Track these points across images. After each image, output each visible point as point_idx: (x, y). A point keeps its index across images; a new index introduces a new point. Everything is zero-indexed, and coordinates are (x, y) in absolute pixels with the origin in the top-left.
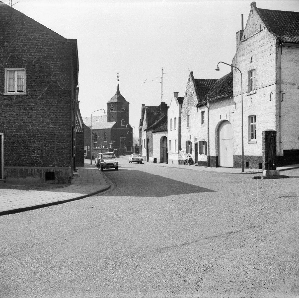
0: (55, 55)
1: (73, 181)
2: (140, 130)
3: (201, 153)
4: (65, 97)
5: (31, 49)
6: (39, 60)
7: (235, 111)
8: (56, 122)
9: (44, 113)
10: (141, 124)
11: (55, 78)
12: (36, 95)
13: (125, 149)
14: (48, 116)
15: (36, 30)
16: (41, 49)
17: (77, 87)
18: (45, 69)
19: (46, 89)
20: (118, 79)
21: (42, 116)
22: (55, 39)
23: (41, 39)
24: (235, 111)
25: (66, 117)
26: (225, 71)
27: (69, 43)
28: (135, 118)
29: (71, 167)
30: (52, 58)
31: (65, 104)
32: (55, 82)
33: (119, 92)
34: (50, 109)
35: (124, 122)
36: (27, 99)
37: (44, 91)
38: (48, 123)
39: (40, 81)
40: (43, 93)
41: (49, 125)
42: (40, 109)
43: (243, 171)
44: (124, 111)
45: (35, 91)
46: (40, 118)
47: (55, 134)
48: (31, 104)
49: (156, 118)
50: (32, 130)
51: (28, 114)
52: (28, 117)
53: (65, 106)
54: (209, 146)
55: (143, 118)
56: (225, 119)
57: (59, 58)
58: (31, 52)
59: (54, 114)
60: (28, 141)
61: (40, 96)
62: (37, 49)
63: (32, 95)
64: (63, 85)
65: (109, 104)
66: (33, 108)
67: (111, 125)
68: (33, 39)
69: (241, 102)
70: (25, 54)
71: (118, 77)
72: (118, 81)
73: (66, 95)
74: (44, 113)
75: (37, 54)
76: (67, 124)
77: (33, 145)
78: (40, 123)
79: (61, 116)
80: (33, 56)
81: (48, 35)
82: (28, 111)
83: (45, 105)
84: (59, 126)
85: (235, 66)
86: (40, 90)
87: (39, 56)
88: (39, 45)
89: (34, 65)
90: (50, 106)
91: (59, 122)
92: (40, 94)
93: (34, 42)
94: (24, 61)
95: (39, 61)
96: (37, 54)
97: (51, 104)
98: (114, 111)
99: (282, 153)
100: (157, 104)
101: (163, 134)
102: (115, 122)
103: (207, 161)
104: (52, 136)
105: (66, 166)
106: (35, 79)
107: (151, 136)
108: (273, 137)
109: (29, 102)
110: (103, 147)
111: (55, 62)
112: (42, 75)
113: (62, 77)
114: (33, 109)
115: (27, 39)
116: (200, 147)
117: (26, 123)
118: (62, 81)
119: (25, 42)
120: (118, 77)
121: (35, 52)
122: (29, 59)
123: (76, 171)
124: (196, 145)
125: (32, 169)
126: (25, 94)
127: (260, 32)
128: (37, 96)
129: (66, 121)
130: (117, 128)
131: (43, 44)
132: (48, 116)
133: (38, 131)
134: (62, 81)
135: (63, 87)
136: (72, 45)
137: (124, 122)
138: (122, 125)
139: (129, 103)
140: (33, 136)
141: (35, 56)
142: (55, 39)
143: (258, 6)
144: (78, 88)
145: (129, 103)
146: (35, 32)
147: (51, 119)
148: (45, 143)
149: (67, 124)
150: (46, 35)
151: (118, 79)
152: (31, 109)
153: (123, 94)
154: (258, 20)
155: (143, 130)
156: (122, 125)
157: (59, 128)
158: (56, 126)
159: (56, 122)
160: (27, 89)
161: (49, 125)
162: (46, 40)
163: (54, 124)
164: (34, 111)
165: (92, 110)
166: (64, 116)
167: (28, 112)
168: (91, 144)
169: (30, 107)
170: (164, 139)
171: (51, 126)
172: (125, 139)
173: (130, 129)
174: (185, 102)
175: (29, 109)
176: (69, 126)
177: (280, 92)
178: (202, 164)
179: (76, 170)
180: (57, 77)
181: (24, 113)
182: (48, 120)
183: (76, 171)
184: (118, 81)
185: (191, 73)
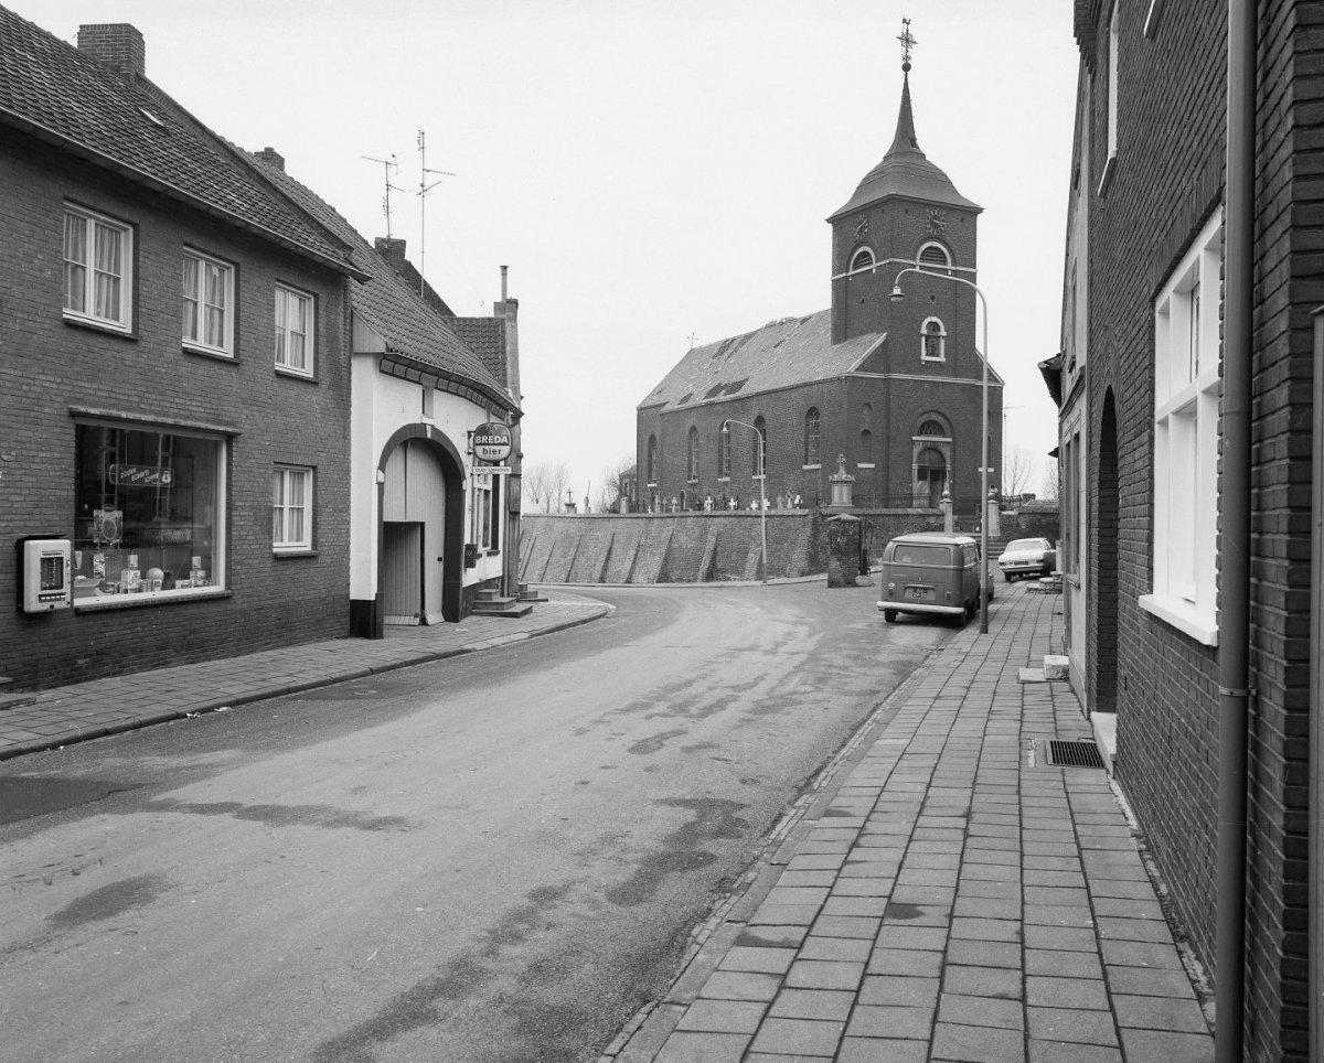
20: (907, 58)
33: (913, 141)
35: (943, 333)
44: (945, 262)
65: (837, 221)
67: (847, 360)
71: (907, 40)
72: (907, 68)
98: (875, 264)
99: (393, 617)
102: (880, 331)
103: (1051, 497)
116: (1154, 28)
120: (907, 40)
130: (888, 370)
137: (943, 333)
138: (924, 357)
139: (980, 210)
145: (980, 210)
151: (907, 58)
153: (928, 142)
156: (924, 357)
168: (277, 344)
172: (947, 453)
184: (907, 68)
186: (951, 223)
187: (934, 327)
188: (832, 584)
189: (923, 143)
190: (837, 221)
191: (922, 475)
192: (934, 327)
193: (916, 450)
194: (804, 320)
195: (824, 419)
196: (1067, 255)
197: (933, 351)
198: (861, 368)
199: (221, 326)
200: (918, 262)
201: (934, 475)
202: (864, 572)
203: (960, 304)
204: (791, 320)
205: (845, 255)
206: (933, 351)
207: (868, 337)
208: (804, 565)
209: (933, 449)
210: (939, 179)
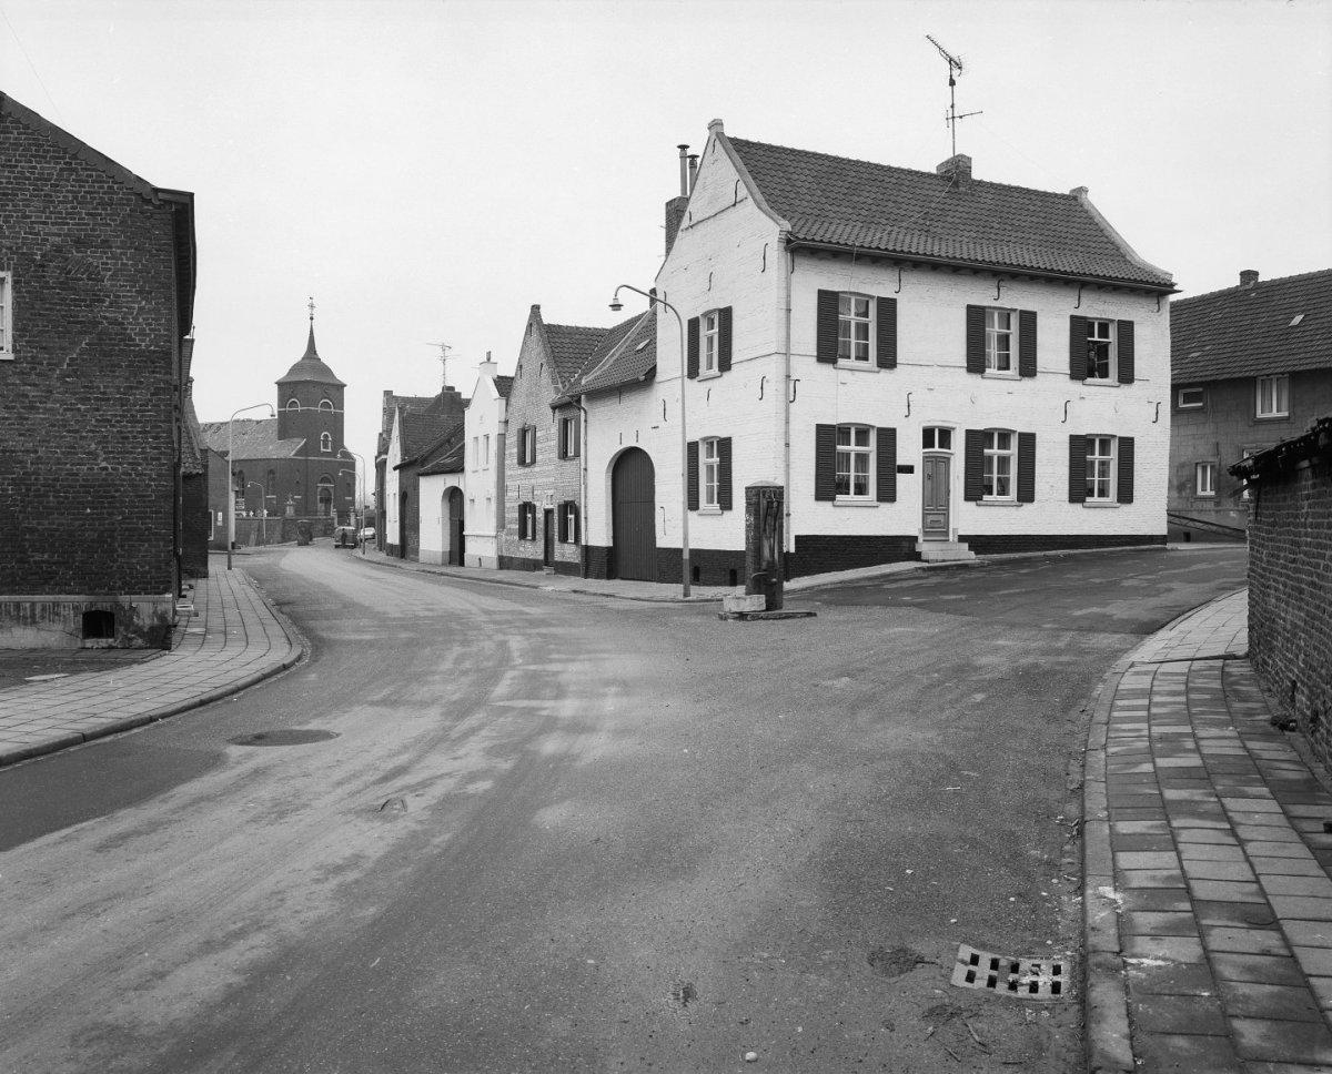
0: (118, 236)
1: (175, 638)
2: (381, 467)
3: (564, 539)
4: (154, 372)
5: (30, 211)
6: (59, 249)
7: (662, 424)
8: (119, 453)
9: (77, 422)
10: (383, 449)
11: (115, 312)
12: (49, 364)
13: (333, 519)
14: (92, 431)
15: (48, 151)
16: (67, 213)
17: (187, 337)
18: (82, 279)
19: (83, 345)
21: (69, 431)
22: (116, 186)
23: (68, 181)
24: (662, 424)
25: (155, 438)
26: (636, 306)
27: (164, 201)
28: (362, 431)
29: (171, 595)
30: (106, 244)
31: (152, 395)
32: (114, 322)
34: (98, 410)
36: (14, 373)
37: (78, 351)
38: (93, 455)
39: (63, 316)
40: (75, 356)
41: (95, 459)
42: (65, 410)
43: (686, 595)
45: (45, 348)
46: (65, 436)
47: (116, 491)
48: (32, 392)
49: (431, 433)
50: (33, 478)
51: (22, 424)
52: (20, 435)
53: (150, 400)
54: (586, 518)
55: (388, 431)
56: (634, 444)
57: (129, 248)
58: (32, 223)
59: (113, 426)
60: (20, 512)
61: (65, 367)
62: (51, 212)
63: (34, 361)
64: (145, 335)
65: (280, 384)
66: (38, 404)
67: (289, 450)
68: (38, 179)
69: (680, 401)
70: (8, 227)
71: (312, 306)
73: (156, 367)
74: (77, 422)
75: (54, 229)
76: (159, 459)
77: (39, 524)
78: (63, 453)
79: (140, 433)
80: (38, 234)
81: (93, 170)
82: (19, 413)
83: (83, 395)
84: (129, 464)
85: (663, 299)
86: (62, 349)
87: (59, 235)
88: (59, 202)
89: (42, 266)
90: (97, 399)
91: (132, 453)
92: (64, 360)
93: (42, 190)
94: (4, 250)
95: (61, 251)
96: (54, 229)
97: (104, 393)
98: (299, 409)
100: (432, 391)
101: (451, 481)
104: (106, 497)
105: (156, 594)
106: (47, 309)
107: (416, 488)
108: (775, 504)
109: (26, 384)
110: (266, 512)
111: (115, 250)
112: (72, 300)
113: (141, 309)
114: (38, 408)
115: (15, 178)
117: (13, 452)
118: (141, 320)
119: (8, 189)
120: (312, 306)
121: (45, 223)
122: (24, 244)
123: (185, 597)
124: (548, 512)
125: (33, 604)
126: (11, 357)
127: (734, 205)
128: (53, 366)
129: (155, 448)
131: (76, 198)
132: (92, 431)
133: (57, 480)
134: (141, 320)
135: (144, 341)
136: (177, 211)
140: (40, 496)
141: (46, 234)
142: (116, 186)
143: (729, 132)
144: (193, 341)
146: (45, 157)
147: (103, 441)
148: (81, 519)
149: (159, 459)
150: (86, 169)
152: (32, 408)
153: (323, 354)
154: (724, 175)
155: (389, 467)
156: (322, 449)
157: (133, 469)
158: (120, 464)
159: (119, 453)
160: (15, 340)
161: (95, 459)
162: (84, 187)
163: (114, 458)
164: (42, 416)
165: (230, 386)
166: (149, 432)
167: (21, 418)
169: (27, 401)
170: (454, 497)
171: (104, 464)
172: (332, 491)
173: (349, 463)
174: (520, 389)
175: (24, 408)
176: (164, 464)
177: (788, 376)
178: (565, 569)
179: (183, 593)
180: (124, 309)
181: (7, 419)
182: (93, 446)
183: (185, 597)
184: (312, 319)
185: (536, 309)
186: (333, 390)
187: (326, 436)
188: (1256, 274)
189: (320, 354)
190: (280, 384)
191: (321, 501)
192: (326, 436)
193: (319, 489)
194: (258, 422)
195: (277, 475)
196: (202, 703)
197: (326, 447)
198: (296, 455)
199: (1124, 731)
200: (319, 409)
201: (326, 501)
202: (311, 540)
203: (336, 424)
204: (250, 421)
205: (282, 401)
206: (326, 447)
207: (296, 440)
208: (280, 539)
209: (326, 489)
210: (326, 371)
